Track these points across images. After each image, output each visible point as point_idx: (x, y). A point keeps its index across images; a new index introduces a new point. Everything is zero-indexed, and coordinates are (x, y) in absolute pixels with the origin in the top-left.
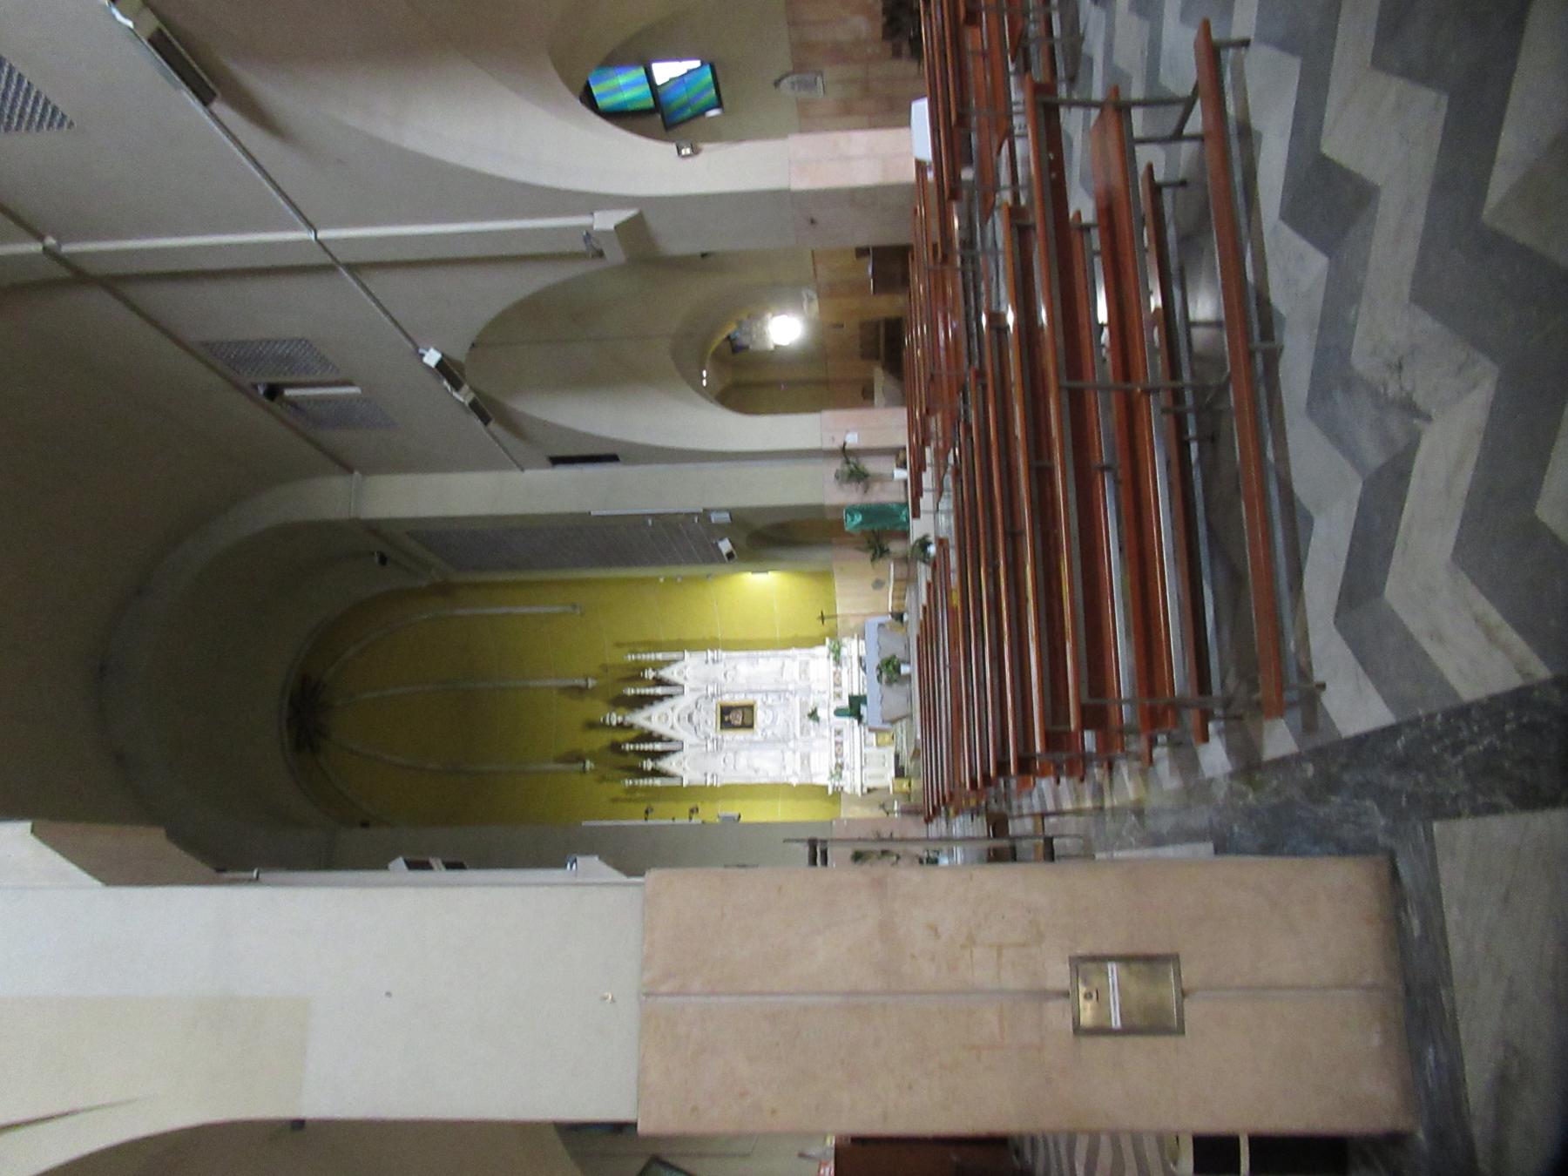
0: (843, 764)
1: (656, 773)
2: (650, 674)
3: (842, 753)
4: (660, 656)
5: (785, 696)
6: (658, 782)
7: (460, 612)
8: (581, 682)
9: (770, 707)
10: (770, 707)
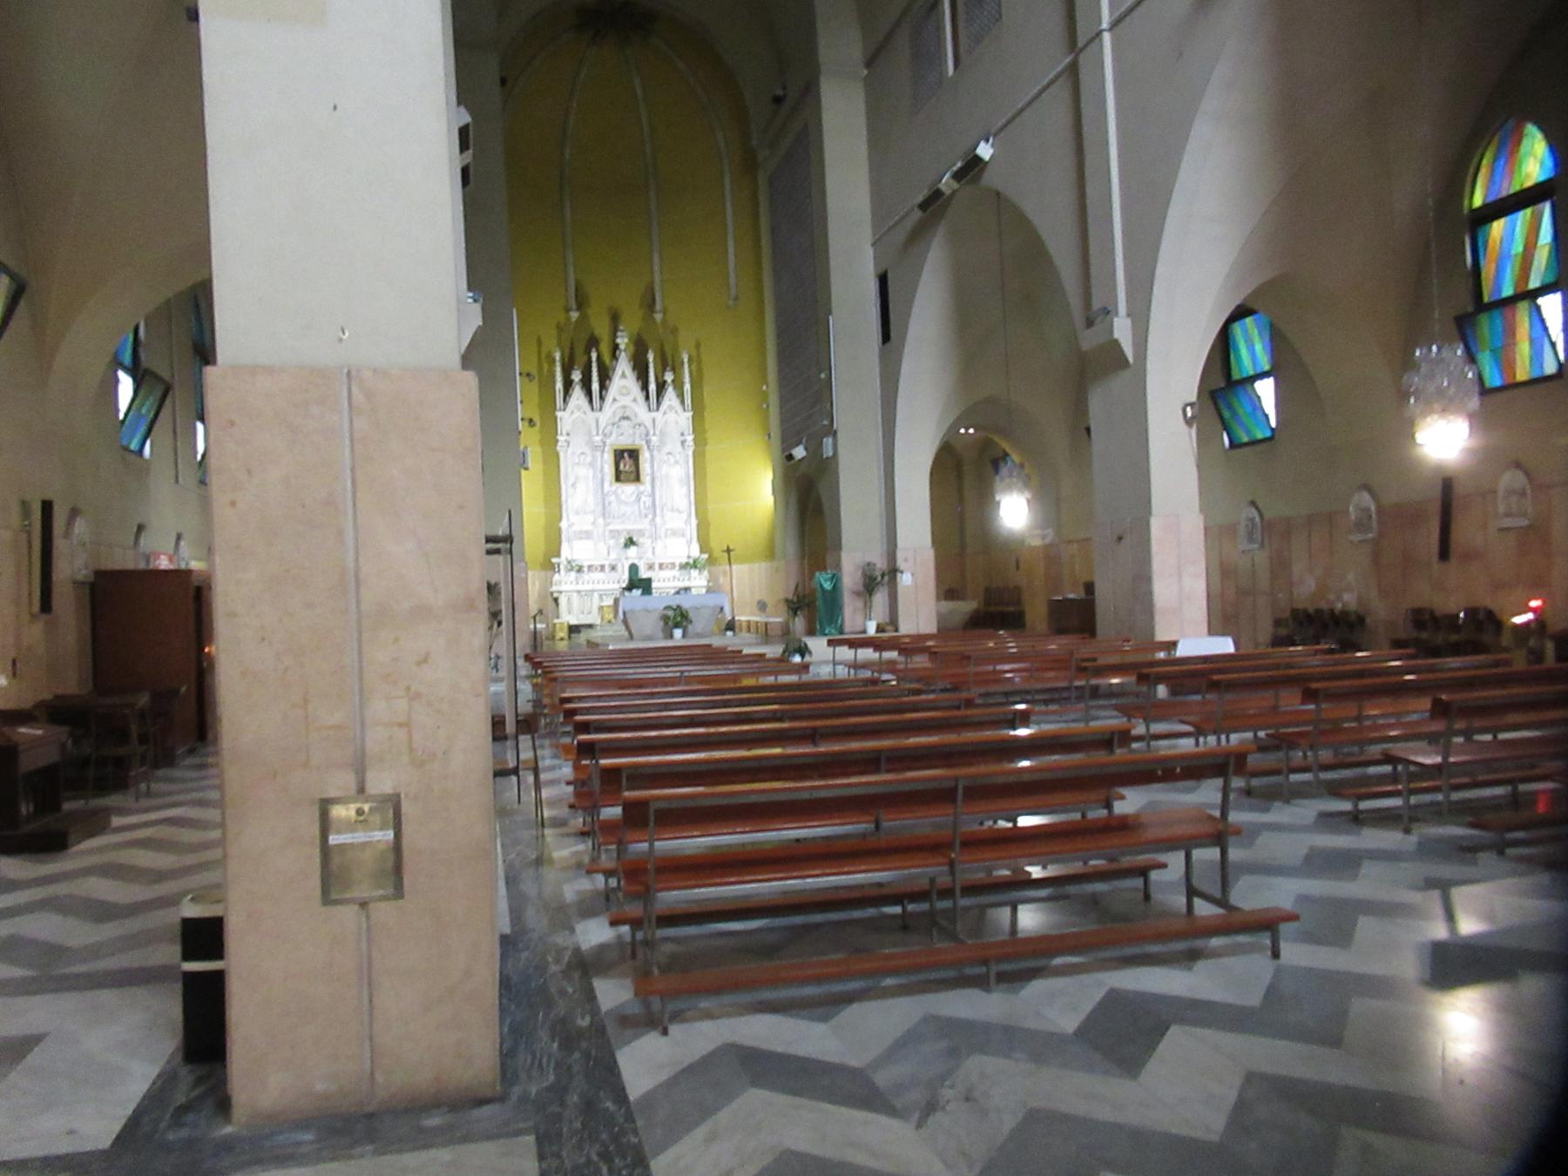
2: (669, 377)
4: (687, 387)
6: (559, 385)
8: (658, 306)
9: (638, 499)
10: (638, 499)
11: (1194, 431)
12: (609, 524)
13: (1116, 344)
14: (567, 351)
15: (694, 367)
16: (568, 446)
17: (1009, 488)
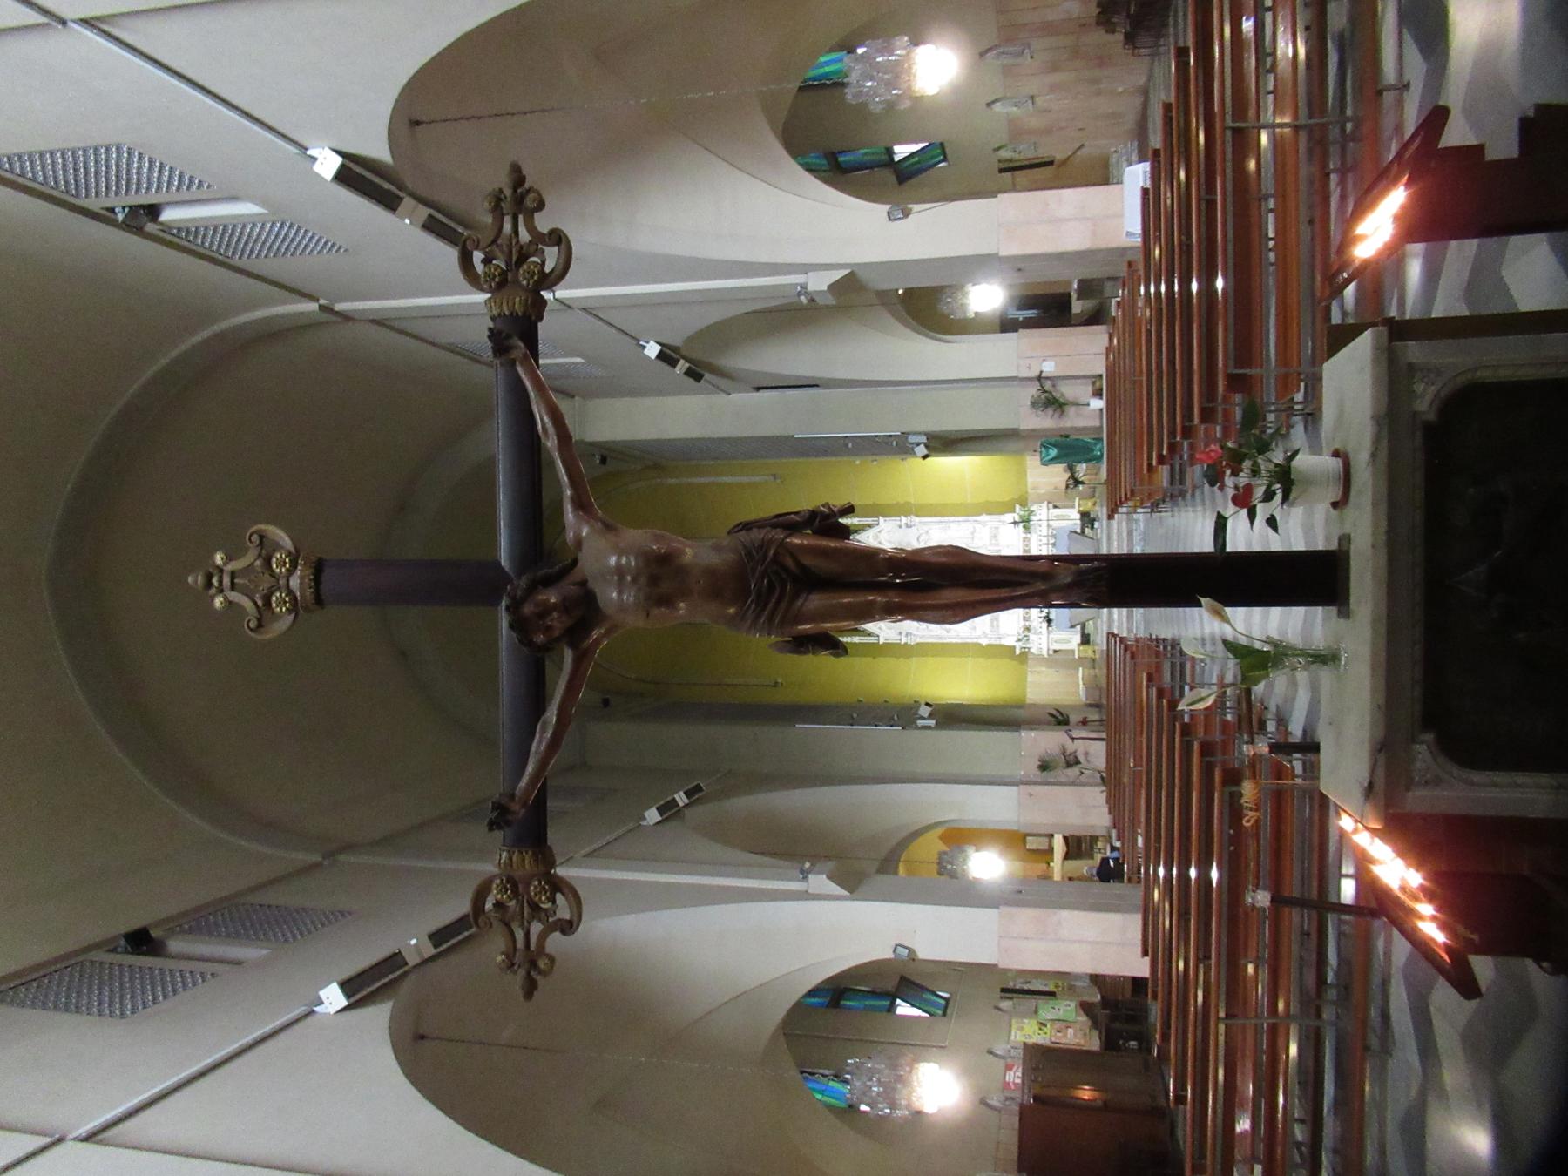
11: (916, 207)
13: (832, 287)
16: (911, 634)
17: (963, 307)
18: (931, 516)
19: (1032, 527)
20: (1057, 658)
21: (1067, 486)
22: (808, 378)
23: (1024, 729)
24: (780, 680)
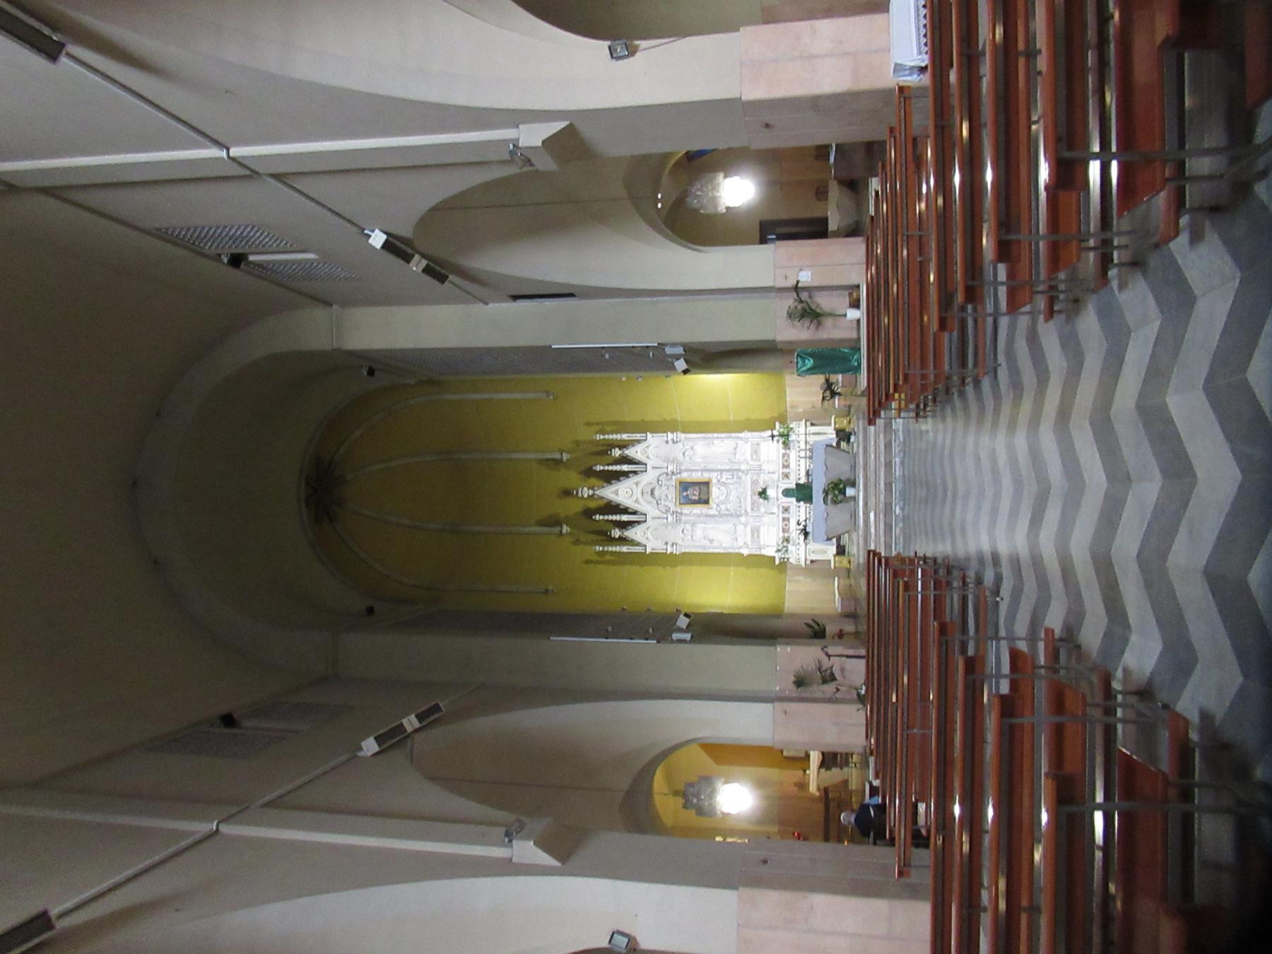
0: (789, 537)
1: (623, 540)
2: (617, 453)
3: (789, 528)
4: (625, 437)
5: (737, 475)
6: (625, 549)
7: (449, 397)
8: (557, 456)
11: (643, 44)
12: (746, 511)
14: (595, 537)
15: (608, 429)
17: (714, 200)
18: (696, 433)
19: (792, 444)
20: (814, 568)
21: (824, 398)
22: (562, 284)
23: (781, 644)
24: (551, 588)
